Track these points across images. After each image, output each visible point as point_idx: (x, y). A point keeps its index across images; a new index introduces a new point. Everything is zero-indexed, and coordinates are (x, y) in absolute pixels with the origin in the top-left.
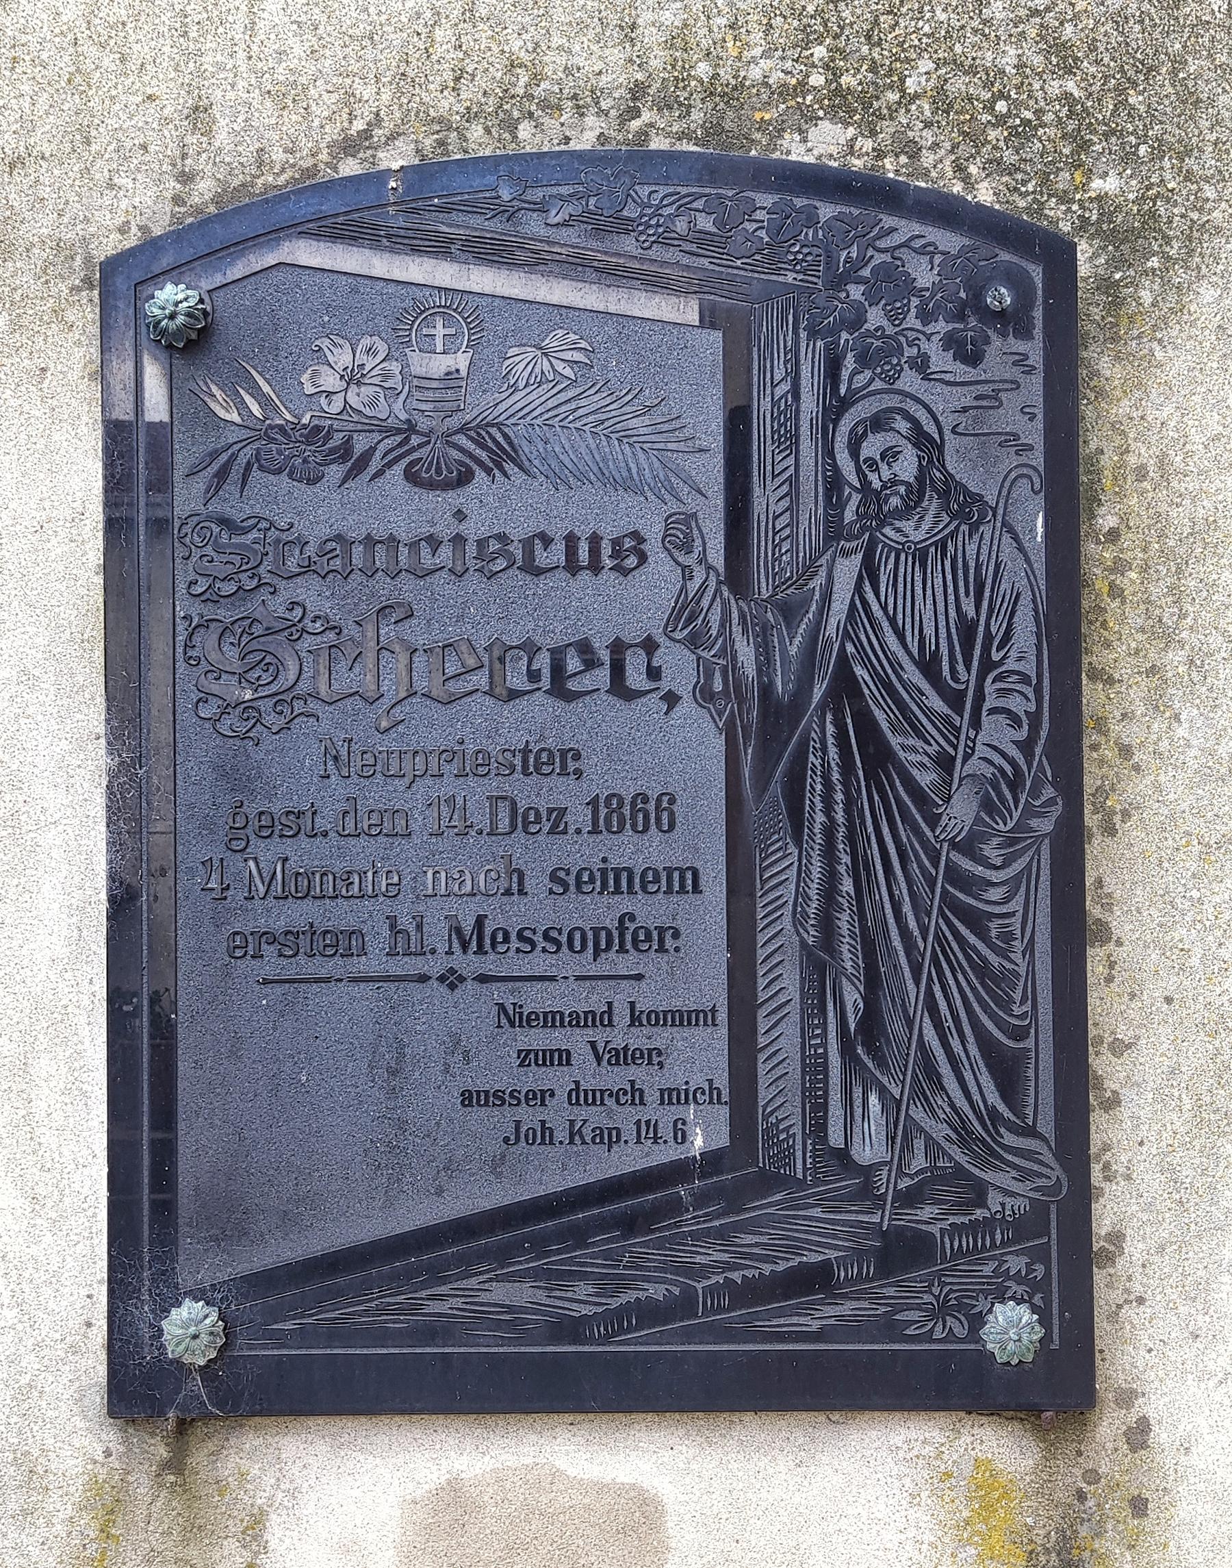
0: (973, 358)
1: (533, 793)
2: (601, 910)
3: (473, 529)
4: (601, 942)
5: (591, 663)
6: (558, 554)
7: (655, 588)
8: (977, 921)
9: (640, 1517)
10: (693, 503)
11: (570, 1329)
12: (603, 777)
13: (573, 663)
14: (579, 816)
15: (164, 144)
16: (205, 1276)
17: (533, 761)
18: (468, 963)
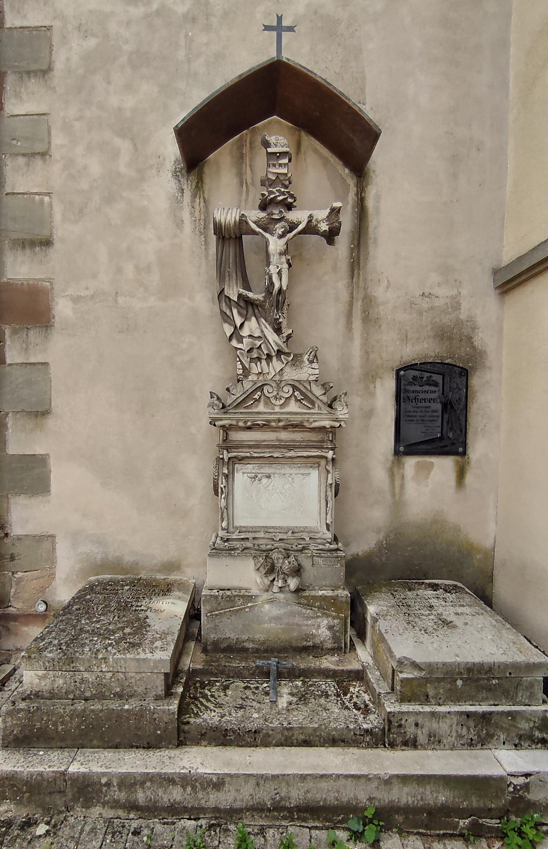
2: (431, 419)
4: (431, 421)
15: (399, 360)
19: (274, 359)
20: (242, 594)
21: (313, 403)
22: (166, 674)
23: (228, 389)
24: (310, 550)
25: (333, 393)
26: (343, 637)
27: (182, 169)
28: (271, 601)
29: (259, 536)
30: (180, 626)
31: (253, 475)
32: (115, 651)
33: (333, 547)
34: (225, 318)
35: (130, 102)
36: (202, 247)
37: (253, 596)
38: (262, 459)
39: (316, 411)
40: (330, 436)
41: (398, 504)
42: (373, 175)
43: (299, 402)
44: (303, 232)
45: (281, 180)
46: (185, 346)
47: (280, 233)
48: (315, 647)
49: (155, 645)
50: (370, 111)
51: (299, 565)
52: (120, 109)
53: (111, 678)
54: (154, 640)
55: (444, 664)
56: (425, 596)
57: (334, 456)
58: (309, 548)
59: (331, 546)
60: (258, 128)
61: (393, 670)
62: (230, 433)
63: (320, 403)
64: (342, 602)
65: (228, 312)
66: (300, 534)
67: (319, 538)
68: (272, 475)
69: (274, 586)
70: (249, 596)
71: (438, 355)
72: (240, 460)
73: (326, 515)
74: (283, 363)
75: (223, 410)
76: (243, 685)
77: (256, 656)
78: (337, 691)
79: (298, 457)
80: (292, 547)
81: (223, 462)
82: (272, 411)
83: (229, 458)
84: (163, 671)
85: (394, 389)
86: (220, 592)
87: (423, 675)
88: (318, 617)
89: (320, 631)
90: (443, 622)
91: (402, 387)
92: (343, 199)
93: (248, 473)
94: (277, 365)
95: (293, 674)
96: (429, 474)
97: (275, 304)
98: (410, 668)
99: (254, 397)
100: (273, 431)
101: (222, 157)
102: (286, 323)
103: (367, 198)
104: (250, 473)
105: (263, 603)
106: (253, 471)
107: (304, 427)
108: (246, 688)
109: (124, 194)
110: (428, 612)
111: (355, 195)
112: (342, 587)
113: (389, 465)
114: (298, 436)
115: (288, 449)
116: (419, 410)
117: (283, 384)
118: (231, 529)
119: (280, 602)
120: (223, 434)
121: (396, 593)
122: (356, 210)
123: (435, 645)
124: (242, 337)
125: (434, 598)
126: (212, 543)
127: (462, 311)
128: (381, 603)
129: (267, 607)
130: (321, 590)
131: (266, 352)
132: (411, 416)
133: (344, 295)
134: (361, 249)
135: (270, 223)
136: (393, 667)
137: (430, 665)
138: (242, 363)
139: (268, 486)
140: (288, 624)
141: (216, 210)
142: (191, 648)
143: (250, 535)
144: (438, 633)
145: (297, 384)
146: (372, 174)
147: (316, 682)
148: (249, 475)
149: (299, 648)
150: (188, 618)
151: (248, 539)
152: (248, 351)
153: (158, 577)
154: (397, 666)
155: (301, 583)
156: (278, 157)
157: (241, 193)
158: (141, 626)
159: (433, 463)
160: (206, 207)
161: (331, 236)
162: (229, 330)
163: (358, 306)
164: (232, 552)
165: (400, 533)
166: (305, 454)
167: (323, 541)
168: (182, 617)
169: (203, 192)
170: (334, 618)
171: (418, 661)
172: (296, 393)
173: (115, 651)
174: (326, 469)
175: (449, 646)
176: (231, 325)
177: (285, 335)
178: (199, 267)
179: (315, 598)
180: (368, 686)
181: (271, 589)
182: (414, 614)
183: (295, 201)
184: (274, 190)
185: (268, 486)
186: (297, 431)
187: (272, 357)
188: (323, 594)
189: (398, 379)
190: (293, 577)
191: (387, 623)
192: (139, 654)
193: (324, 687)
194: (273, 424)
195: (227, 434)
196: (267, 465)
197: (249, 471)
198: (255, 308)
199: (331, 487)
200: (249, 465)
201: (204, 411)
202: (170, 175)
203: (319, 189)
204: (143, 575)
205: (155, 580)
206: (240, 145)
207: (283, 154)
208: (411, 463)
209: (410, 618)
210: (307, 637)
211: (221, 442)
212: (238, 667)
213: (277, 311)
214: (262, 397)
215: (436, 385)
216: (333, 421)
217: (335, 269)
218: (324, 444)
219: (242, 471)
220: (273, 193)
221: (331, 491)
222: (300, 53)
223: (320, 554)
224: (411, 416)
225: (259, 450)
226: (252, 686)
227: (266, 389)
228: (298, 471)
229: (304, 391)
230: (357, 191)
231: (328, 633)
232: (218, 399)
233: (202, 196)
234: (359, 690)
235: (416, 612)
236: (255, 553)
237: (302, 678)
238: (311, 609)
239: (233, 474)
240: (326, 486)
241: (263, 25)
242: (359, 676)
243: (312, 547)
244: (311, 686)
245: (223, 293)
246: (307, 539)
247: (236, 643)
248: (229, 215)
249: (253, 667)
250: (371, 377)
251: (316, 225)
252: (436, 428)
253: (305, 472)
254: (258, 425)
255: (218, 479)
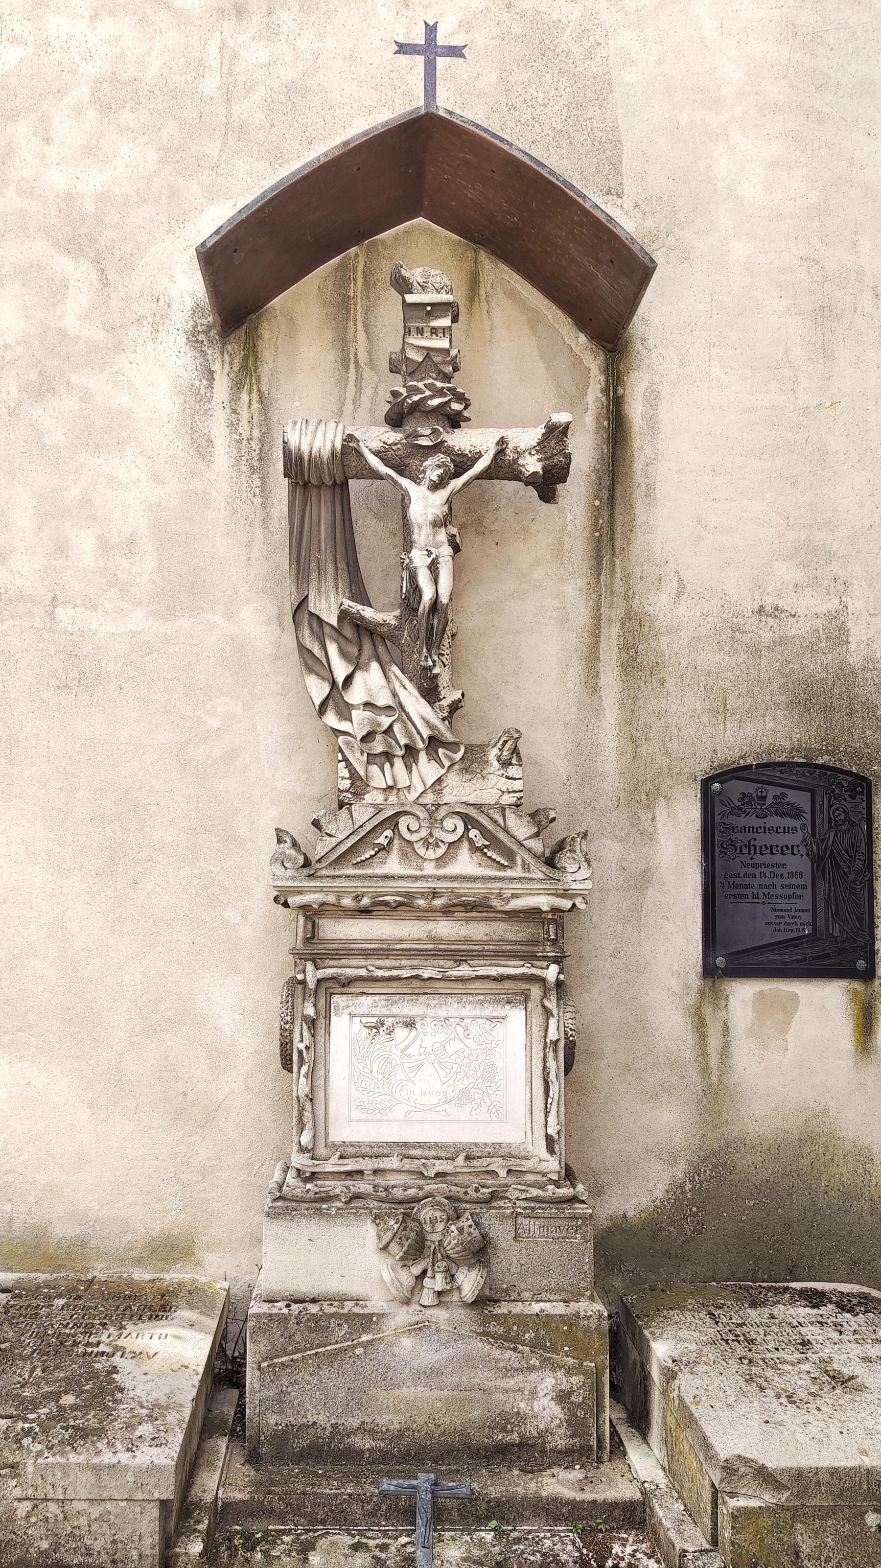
0: (854, 799)
1: (777, 871)
2: (790, 892)
3: (767, 826)
4: (789, 897)
5: (767, 848)
6: (782, 830)
7: (799, 835)
8: (855, 895)
9: (794, 998)
10: (805, 822)
11: (785, 964)
12: (790, 868)
13: (785, 849)
14: (786, 875)
15: (709, 756)
16: (721, 953)
17: (778, 866)
18: (767, 901)
19: (423, 757)
20: (346, 1311)
21: (510, 855)
22: (164, 1504)
23: (316, 824)
24: (510, 1200)
25: (558, 831)
26: (592, 1421)
27: (210, 327)
28: (418, 1328)
29: (388, 1167)
30: (196, 1390)
31: (374, 1020)
32: (39, 1447)
33: (565, 1191)
34: (310, 662)
35: (93, 180)
36: (255, 500)
37: (373, 1315)
38: (394, 984)
39: (517, 872)
40: (549, 933)
41: (715, 1092)
42: (641, 347)
43: (478, 854)
44: (486, 474)
45: (436, 364)
46: (214, 723)
47: (434, 478)
48: (524, 1445)
49: (137, 1433)
50: (627, 221)
51: (484, 1237)
52: (69, 197)
53: (28, 1516)
54: (135, 1421)
55: (834, 1472)
56: (791, 1320)
57: (562, 977)
58: (508, 1194)
59: (560, 1191)
60: (383, 242)
61: (715, 1493)
62: (321, 922)
63: (527, 857)
64: (587, 1330)
65: (317, 651)
66: (486, 1161)
67: (529, 1172)
68: (418, 1020)
69: (425, 1291)
70: (364, 1316)
71: (800, 746)
72: (343, 986)
73: (546, 1116)
74: (442, 766)
75: (306, 871)
76: (348, 1540)
77: (381, 1471)
78: (582, 1554)
79: (478, 978)
80: (466, 1193)
81: (305, 988)
82: (418, 873)
83: (319, 981)
84: (156, 1496)
85: (698, 824)
86: (294, 1307)
87: (783, 1499)
88: (531, 1369)
89: (537, 1406)
90: (833, 1377)
91: (718, 819)
92: (574, 402)
93: (362, 1016)
94: (427, 770)
95: (471, 1513)
96: (788, 1022)
97: (423, 635)
98: (754, 1484)
99: (377, 842)
100: (419, 919)
101: (302, 304)
102: (447, 679)
103: (628, 399)
104: (367, 1016)
105: (397, 1334)
106: (376, 1011)
107: (490, 908)
108: (356, 1547)
109: (75, 379)
110: (797, 1355)
111: (602, 391)
112: (588, 1293)
113: (691, 999)
114: (477, 930)
115: (456, 961)
116: (757, 872)
117: (442, 812)
118: (322, 1151)
119: (438, 1331)
120: (305, 927)
121: (719, 1311)
122: (606, 423)
123: (812, 1429)
124: (349, 707)
125: (812, 1323)
126: (274, 1185)
127: (852, 646)
128: (684, 1333)
129: (407, 1342)
130: (538, 1301)
131: (403, 741)
132: (740, 886)
133: (581, 614)
134: (619, 509)
135: (410, 455)
136: (713, 1485)
137: (799, 1475)
138: (349, 765)
139: (409, 1046)
140: (457, 1387)
141: (290, 424)
142: (218, 1451)
143: (367, 1165)
144: (819, 1402)
145: (473, 813)
146: (638, 346)
147: (530, 1532)
148: (364, 1020)
149: (486, 1449)
150: (209, 1381)
151: (360, 1172)
152: (364, 739)
153: (136, 1276)
154: (722, 1481)
155: (489, 1282)
156: (429, 314)
157: (343, 383)
158: (103, 1390)
159: (796, 995)
160: (265, 411)
161: (547, 486)
162: (318, 690)
163: (611, 634)
164: (324, 1206)
165: (724, 1165)
166: (494, 971)
167: (539, 1177)
168: (201, 1370)
169: (258, 381)
170: (570, 1372)
171: (770, 1465)
172: (473, 833)
173: (39, 1447)
174: (543, 1006)
175: (845, 1431)
176: (323, 679)
177: (445, 703)
178: (249, 544)
179: (522, 1320)
180: (657, 1540)
181: (416, 1299)
182: (763, 1360)
183: (466, 408)
184: (420, 385)
185: (409, 1046)
186: (474, 919)
187: (418, 751)
188: (542, 1311)
189: (708, 801)
190: (470, 1267)
191: (697, 1382)
192: (98, 1453)
193: (548, 1543)
194: (421, 902)
195: (314, 924)
196: (407, 997)
197: (364, 1010)
198: (378, 640)
199: (555, 1051)
200: (363, 998)
201: (258, 873)
202: (182, 339)
203: (519, 375)
204: (100, 1271)
205: (130, 1283)
206: (344, 276)
207: (438, 309)
208: (743, 994)
209: (753, 1368)
210: (507, 1420)
211: (299, 945)
212: (336, 1495)
213: (429, 650)
214: (396, 841)
215: (796, 813)
216: (558, 896)
217: (558, 552)
218: (539, 952)
219: (347, 1011)
220: (418, 391)
221: (556, 1058)
222: (469, 98)
223: (533, 1209)
224: (740, 886)
225: (387, 963)
226: (371, 1543)
227: (403, 822)
228: (477, 1012)
229: (491, 827)
230: (607, 381)
231: (556, 1410)
232: (295, 844)
233: (255, 387)
234: (635, 1551)
235: (769, 1355)
236: (380, 1208)
237: (493, 1524)
238: (515, 1349)
239: (328, 1017)
240: (545, 1048)
241: (396, 42)
242: (635, 1515)
243: (513, 1194)
244: (518, 1541)
245: (305, 605)
246: (503, 1173)
247: (332, 1438)
248: (320, 435)
249: (372, 1495)
250: (644, 797)
251: (515, 461)
252: (800, 914)
253: (495, 1014)
254: (386, 904)
255: (291, 1031)
